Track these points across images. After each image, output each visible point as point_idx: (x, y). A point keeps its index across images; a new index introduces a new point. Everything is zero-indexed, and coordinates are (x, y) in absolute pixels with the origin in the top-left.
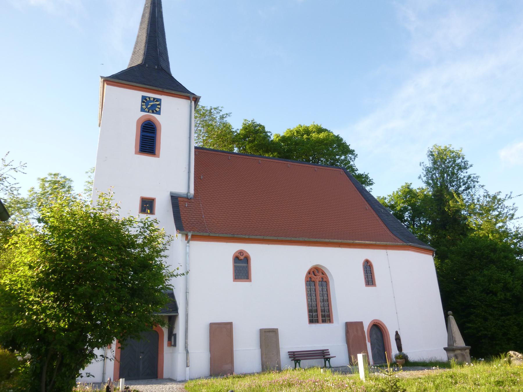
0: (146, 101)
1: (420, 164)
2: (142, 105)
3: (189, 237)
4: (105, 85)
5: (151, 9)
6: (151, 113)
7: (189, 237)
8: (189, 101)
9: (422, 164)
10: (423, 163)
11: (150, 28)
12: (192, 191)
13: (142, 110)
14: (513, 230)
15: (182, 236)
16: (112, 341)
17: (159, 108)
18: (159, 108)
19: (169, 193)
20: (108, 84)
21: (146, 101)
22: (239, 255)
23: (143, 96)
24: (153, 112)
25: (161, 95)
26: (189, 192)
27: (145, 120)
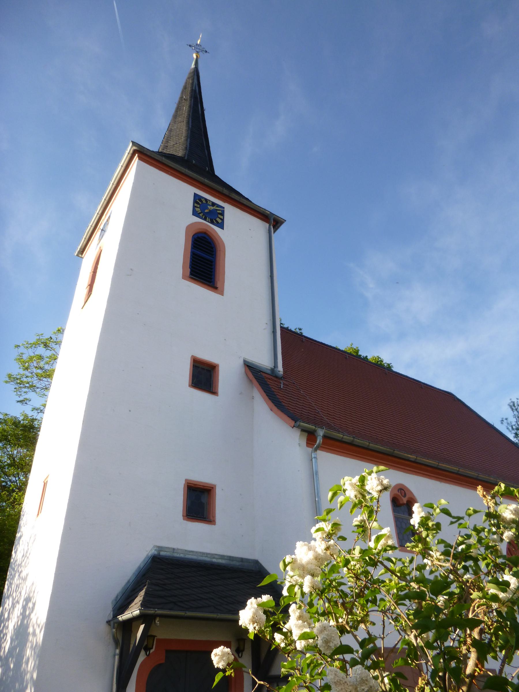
0: (200, 203)
1: (503, 421)
2: (194, 207)
3: (319, 440)
4: (136, 158)
5: (191, 103)
6: (209, 222)
7: (319, 440)
8: (267, 225)
9: (505, 421)
10: (506, 419)
11: (192, 122)
12: (280, 368)
13: (195, 213)
14: (309, 589)
15: (301, 434)
16: (227, 676)
17: (221, 219)
18: (221, 219)
19: (241, 362)
20: (140, 158)
21: (200, 203)
22: (400, 494)
23: (195, 195)
24: (212, 222)
25: (225, 201)
26: (276, 366)
27: (201, 231)
